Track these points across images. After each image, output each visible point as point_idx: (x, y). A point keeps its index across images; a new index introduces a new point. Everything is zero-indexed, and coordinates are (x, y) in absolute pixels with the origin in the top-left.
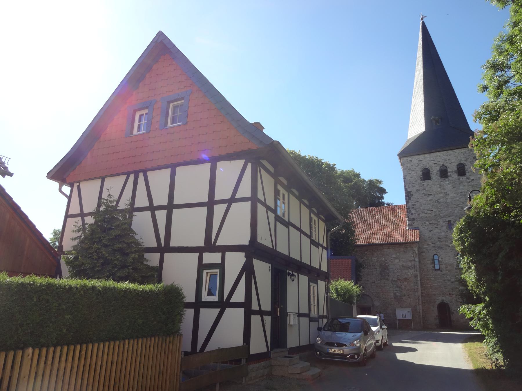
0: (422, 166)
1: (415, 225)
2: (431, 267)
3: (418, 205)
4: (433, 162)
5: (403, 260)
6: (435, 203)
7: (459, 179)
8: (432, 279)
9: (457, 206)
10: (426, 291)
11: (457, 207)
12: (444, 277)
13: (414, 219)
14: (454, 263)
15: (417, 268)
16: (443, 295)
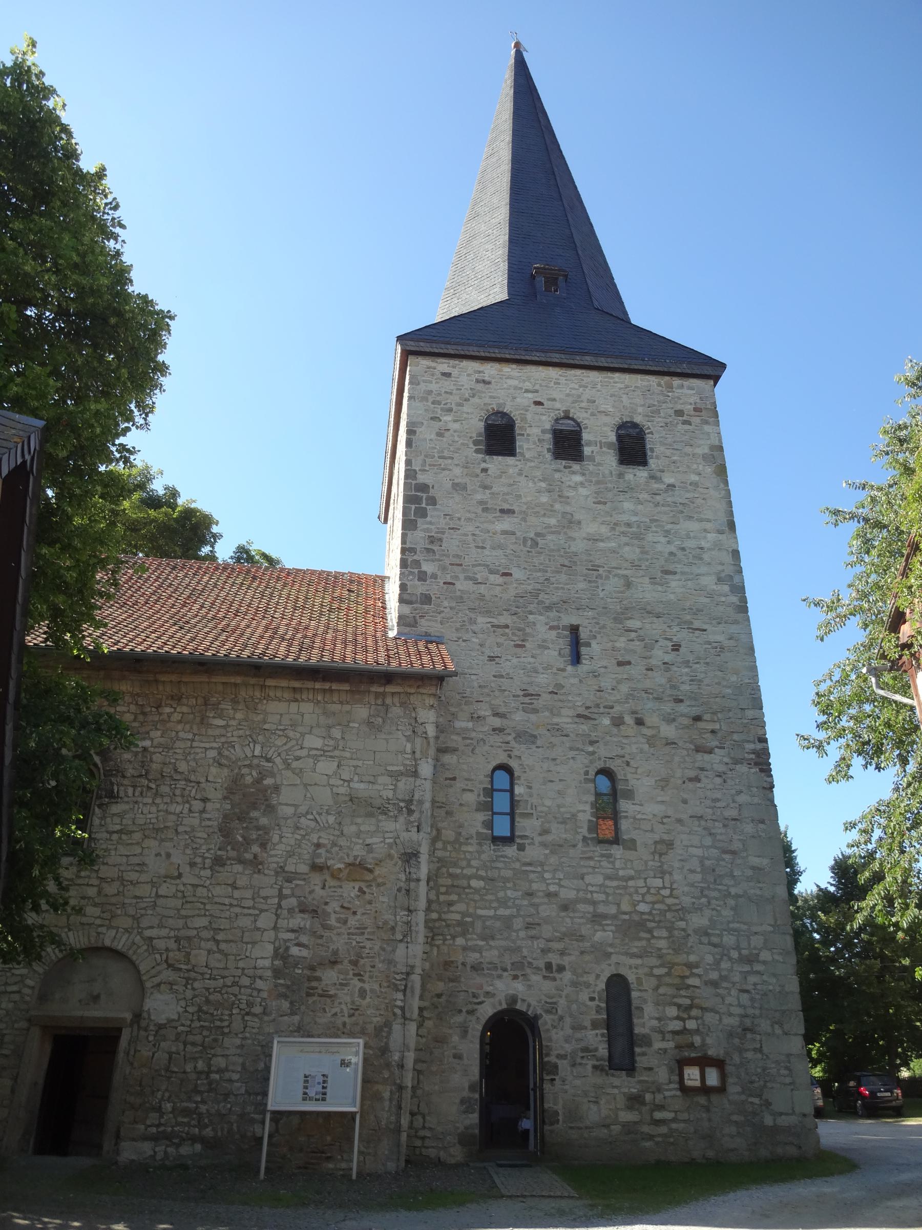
0: (487, 400)
1: (425, 625)
2: (475, 822)
3: (451, 544)
4: (530, 395)
5: (360, 763)
6: (525, 546)
7: (621, 475)
8: (474, 883)
9: (609, 572)
10: (438, 947)
11: (607, 578)
12: (532, 876)
13: (426, 599)
14: (579, 811)
15: (421, 812)
16: (519, 973)
